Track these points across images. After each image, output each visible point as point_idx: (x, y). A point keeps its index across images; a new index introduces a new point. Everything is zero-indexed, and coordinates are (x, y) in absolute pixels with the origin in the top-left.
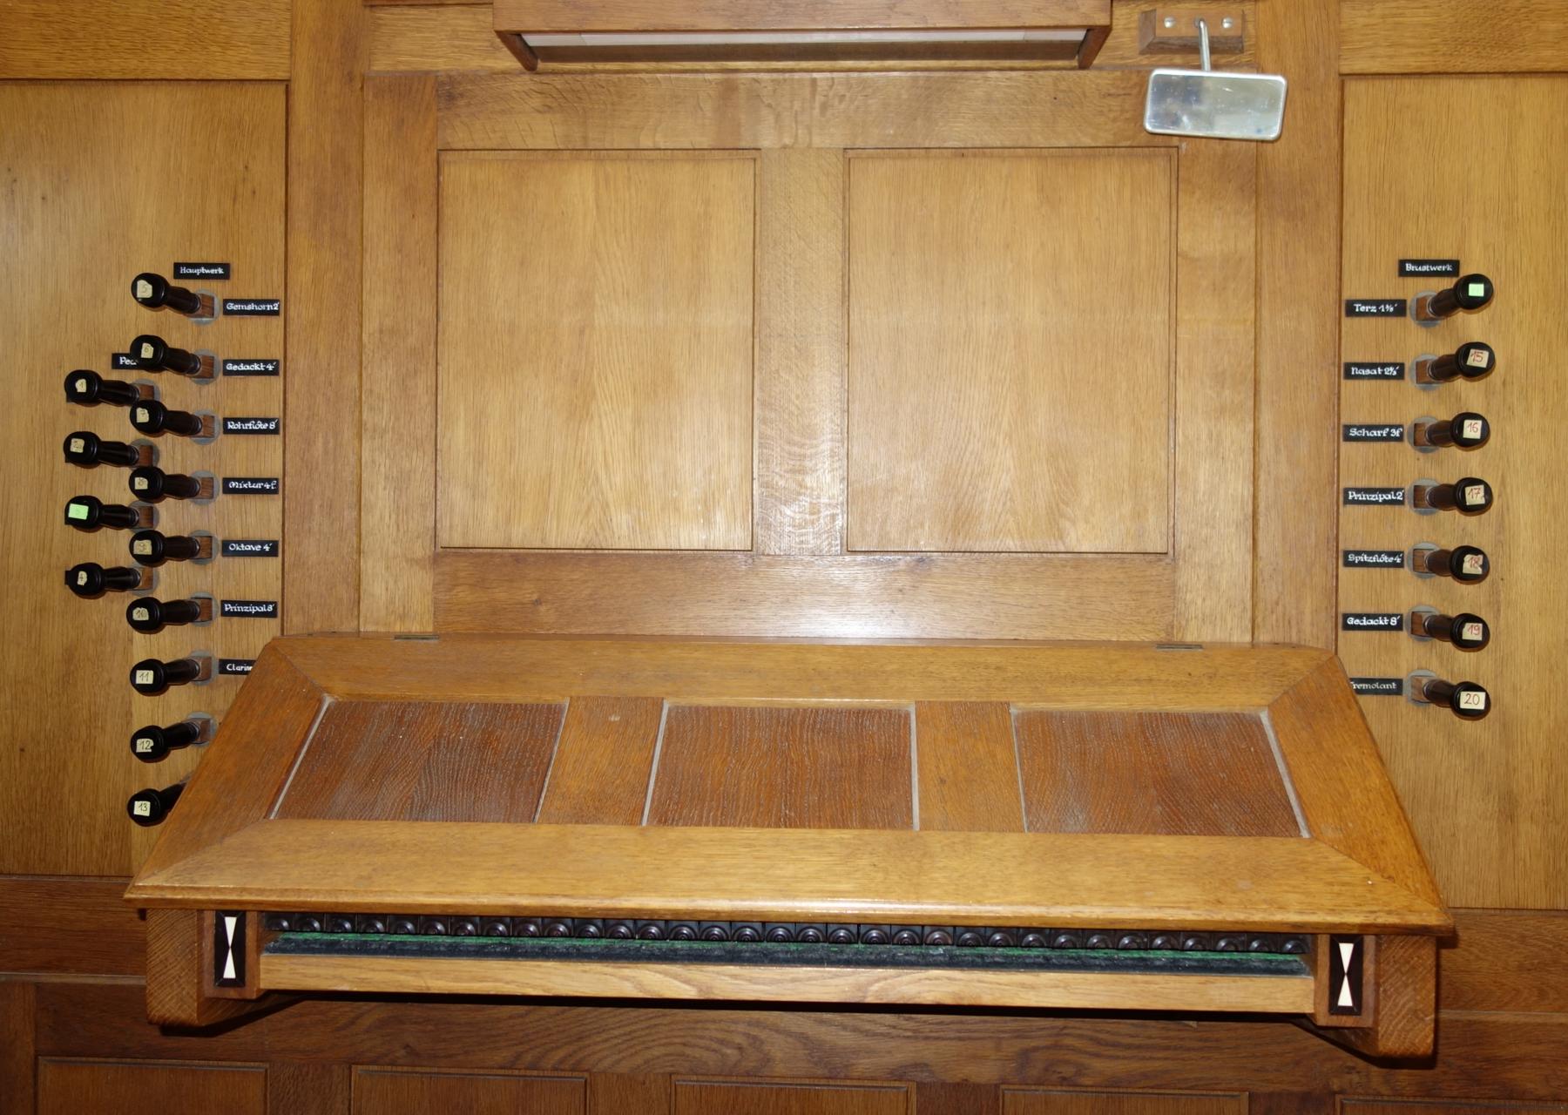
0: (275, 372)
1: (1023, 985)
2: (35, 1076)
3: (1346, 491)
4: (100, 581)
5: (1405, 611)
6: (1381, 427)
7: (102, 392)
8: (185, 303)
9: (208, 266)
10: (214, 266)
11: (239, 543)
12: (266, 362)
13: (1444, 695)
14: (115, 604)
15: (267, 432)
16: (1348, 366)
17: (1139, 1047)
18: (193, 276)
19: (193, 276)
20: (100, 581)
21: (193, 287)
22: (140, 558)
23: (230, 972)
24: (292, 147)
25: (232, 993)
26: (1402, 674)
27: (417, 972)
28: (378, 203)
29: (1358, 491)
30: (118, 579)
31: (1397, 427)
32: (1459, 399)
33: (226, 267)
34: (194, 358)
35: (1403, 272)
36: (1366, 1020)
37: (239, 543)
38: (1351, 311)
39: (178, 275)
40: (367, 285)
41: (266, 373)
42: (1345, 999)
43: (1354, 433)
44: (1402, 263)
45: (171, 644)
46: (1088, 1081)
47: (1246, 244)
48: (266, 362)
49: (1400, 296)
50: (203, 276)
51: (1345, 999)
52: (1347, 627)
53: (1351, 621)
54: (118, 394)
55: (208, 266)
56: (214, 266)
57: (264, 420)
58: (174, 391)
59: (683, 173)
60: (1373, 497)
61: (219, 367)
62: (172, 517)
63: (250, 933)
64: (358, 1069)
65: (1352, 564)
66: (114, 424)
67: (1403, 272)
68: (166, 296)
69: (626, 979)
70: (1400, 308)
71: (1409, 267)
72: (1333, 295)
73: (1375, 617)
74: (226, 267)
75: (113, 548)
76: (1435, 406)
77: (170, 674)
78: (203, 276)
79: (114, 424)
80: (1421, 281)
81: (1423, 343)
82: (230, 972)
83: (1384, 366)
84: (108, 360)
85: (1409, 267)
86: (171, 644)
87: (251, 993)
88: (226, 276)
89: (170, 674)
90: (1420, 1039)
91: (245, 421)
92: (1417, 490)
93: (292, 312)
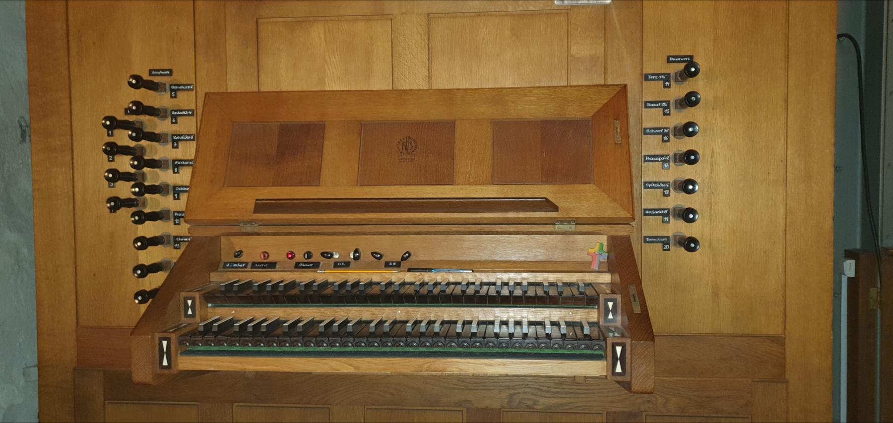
0: (192, 115)
1: (486, 364)
2: (104, 409)
3: (645, 156)
4: (117, 204)
5: (671, 207)
6: (660, 129)
7: (114, 124)
8: (152, 86)
9: (163, 70)
10: (166, 70)
11: (180, 187)
12: (188, 111)
13: (689, 244)
14: (125, 213)
15: (190, 140)
16: (646, 103)
17: (566, 393)
18: (157, 75)
19: (157, 75)
20: (117, 204)
21: (156, 79)
22: (134, 193)
23: (165, 363)
24: (197, 17)
25: (166, 372)
26: (670, 234)
27: (241, 363)
28: (232, 44)
29: (650, 156)
30: (128, 203)
31: (666, 128)
32: (693, 116)
33: (171, 71)
34: (158, 109)
35: (669, 61)
36: (627, 378)
37: (180, 187)
38: (646, 79)
39: (150, 74)
40: (228, 77)
41: (189, 115)
42: (619, 369)
43: (648, 131)
44: (669, 57)
45: (150, 229)
46: (539, 407)
47: (600, 51)
48: (188, 111)
49: (668, 72)
50: (161, 75)
51: (619, 369)
52: (645, 215)
53: (647, 212)
54: (125, 125)
55: (163, 70)
56: (166, 70)
57: (188, 135)
58: (150, 123)
59: (361, 26)
60: (656, 159)
61: (169, 112)
62: (152, 176)
63: (173, 347)
64: (235, 404)
65: (648, 188)
66: (123, 138)
67: (669, 61)
68: (139, 83)
69: (327, 364)
70: (668, 76)
71: (672, 59)
72: (639, 72)
73: (657, 210)
74: (171, 71)
75: (125, 190)
76: (678, 118)
77: (146, 243)
78: (161, 75)
79: (123, 138)
80: (676, 64)
81: (678, 91)
82: (165, 363)
83: (661, 102)
84: (123, 111)
85: (672, 59)
86: (150, 229)
87: (174, 371)
88: (171, 74)
89: (146, 243)
90: (649, 385)
91: (180, 135)
92: (675, 155)
93: (198, 89)
